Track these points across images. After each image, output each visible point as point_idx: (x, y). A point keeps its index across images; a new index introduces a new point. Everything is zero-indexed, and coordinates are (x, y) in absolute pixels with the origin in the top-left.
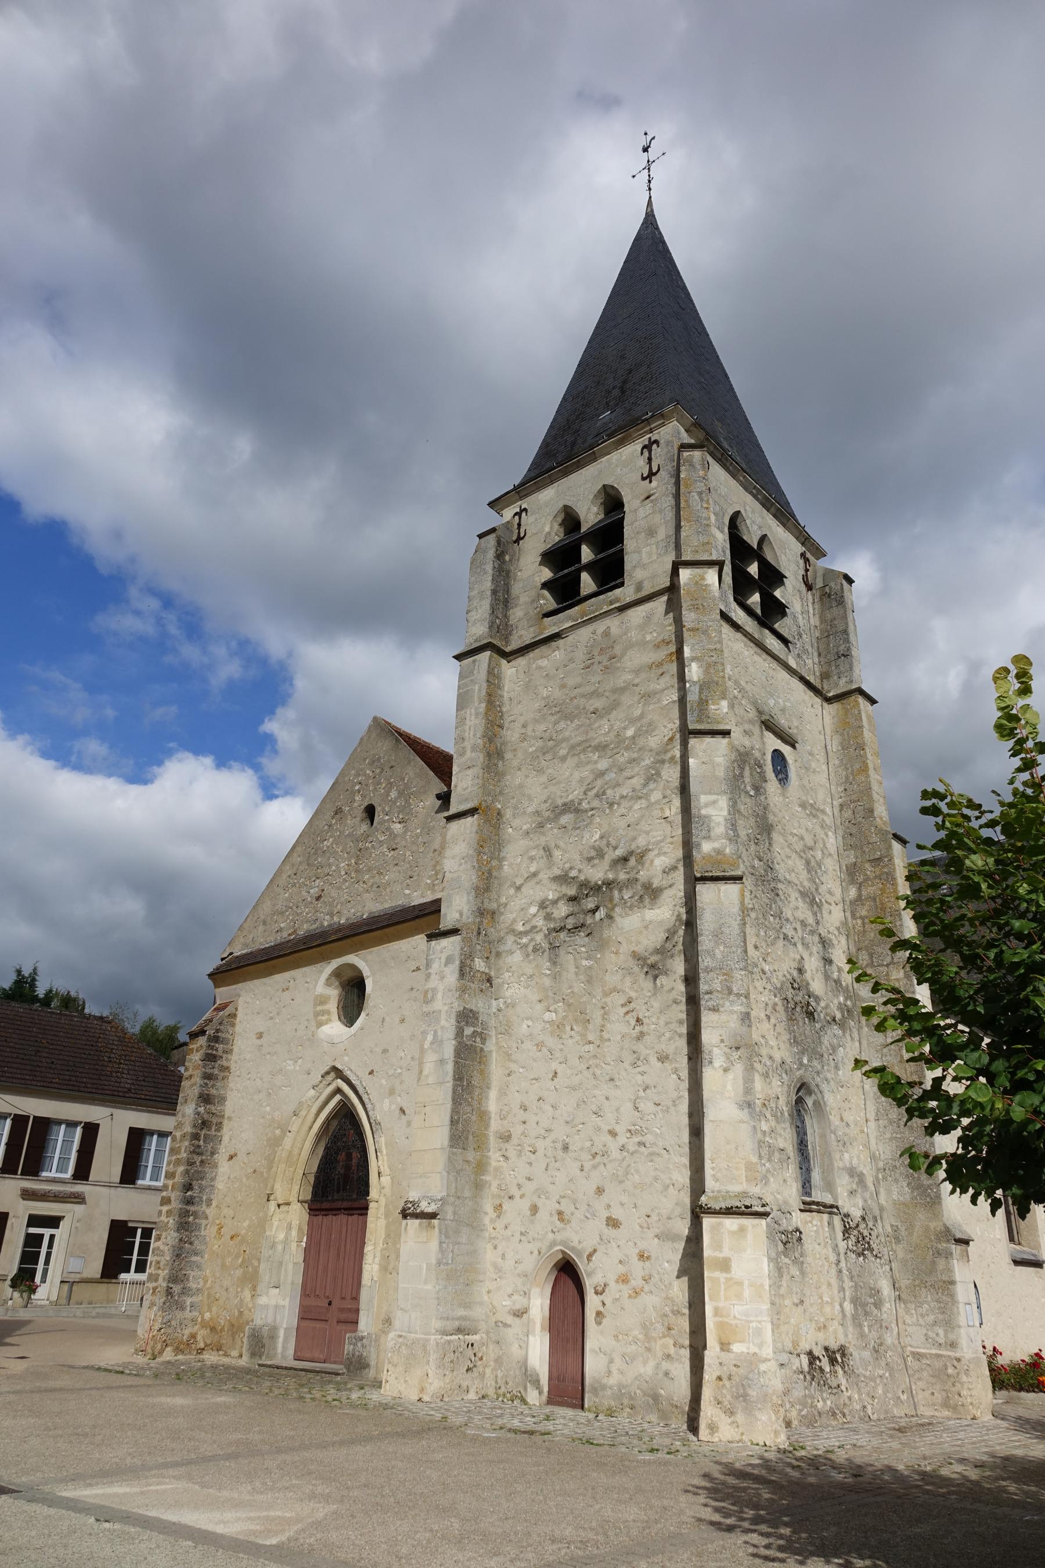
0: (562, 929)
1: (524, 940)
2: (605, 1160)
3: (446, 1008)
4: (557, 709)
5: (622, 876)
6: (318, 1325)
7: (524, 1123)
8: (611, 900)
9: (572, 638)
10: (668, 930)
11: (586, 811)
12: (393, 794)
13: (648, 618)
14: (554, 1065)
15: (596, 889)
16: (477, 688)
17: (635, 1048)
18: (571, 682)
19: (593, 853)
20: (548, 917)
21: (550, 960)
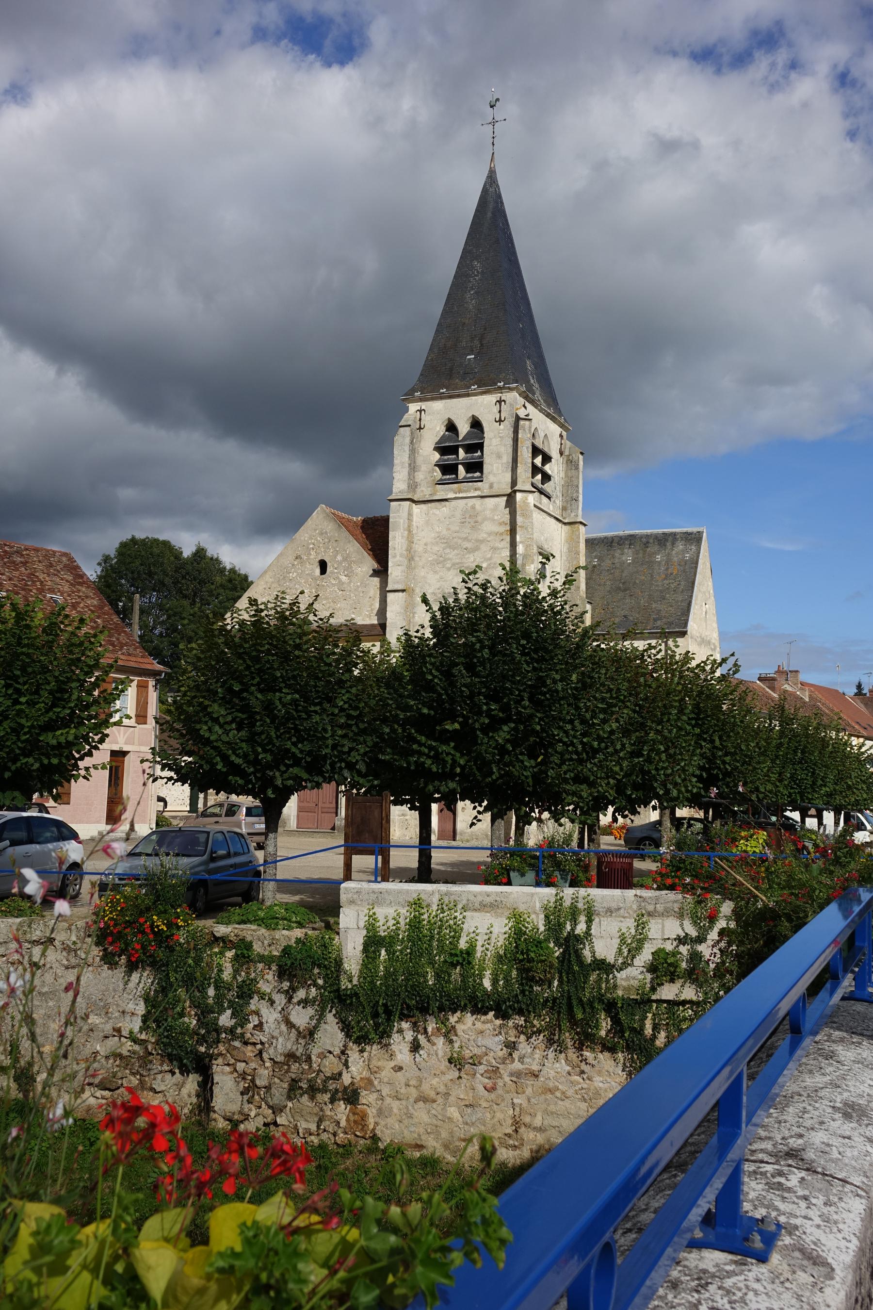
6: (310, 814)
9: (454, 503)
12: (339, 558)
13: (496, 506)
16: (402, 521)
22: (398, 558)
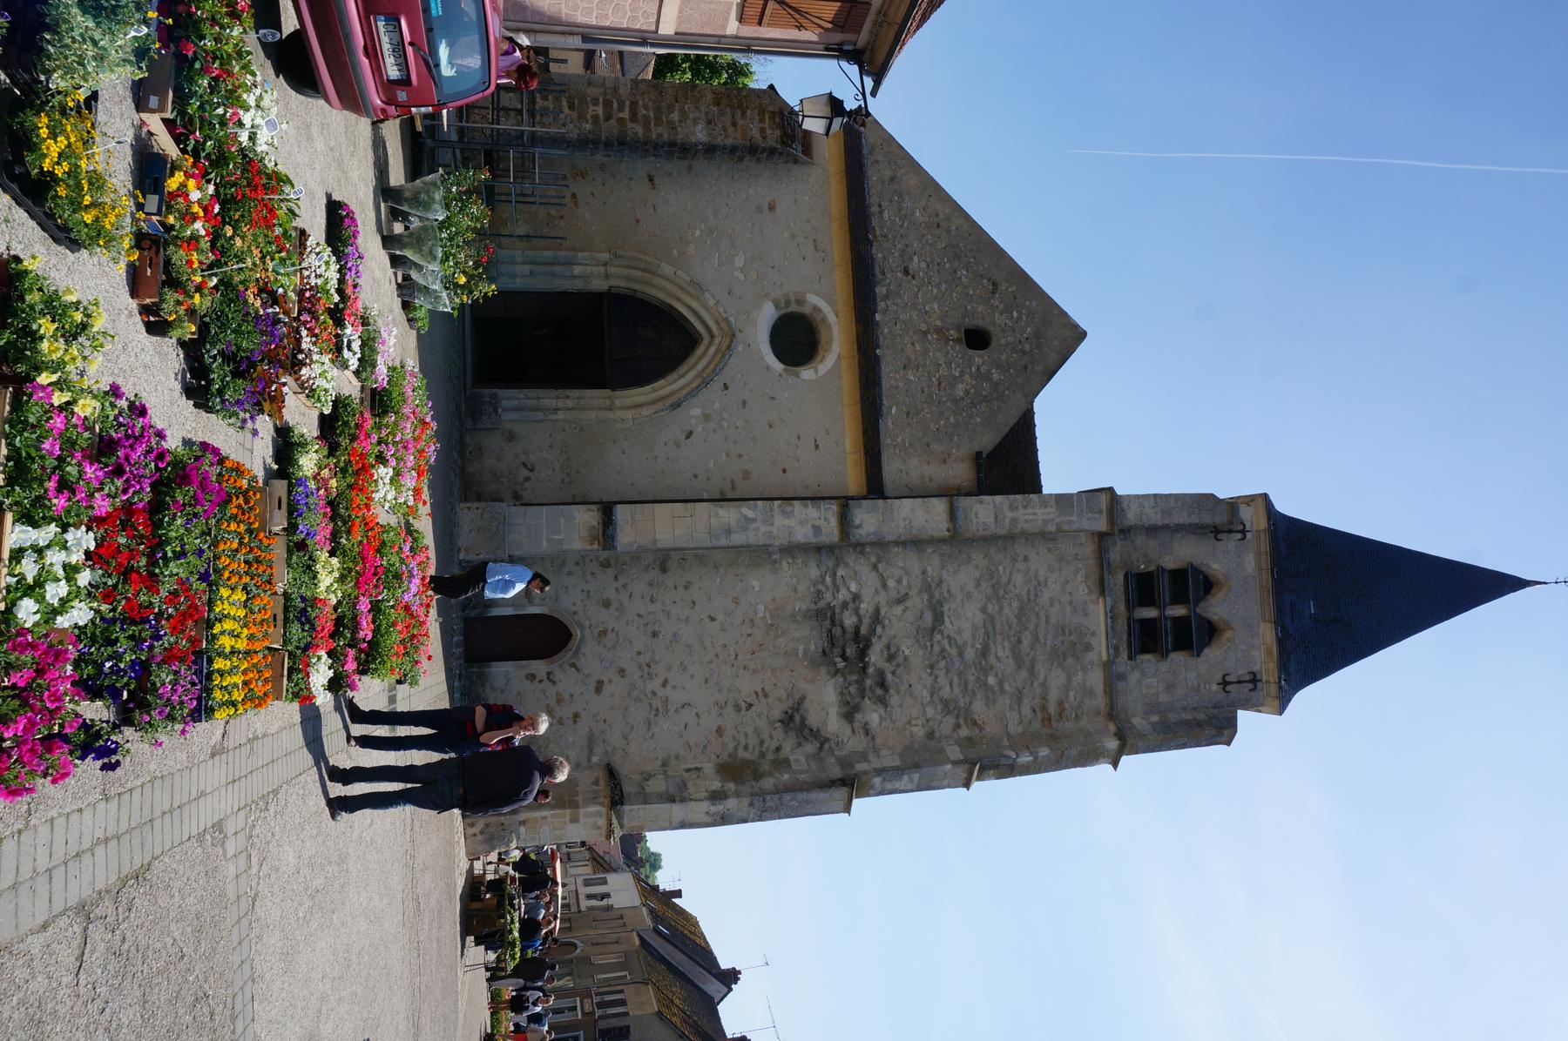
0: (833, 621)
1: (828, 579)
2: (646, 676)
3: (775, 531)
4: (1032, 598)
5: (868, 682)
7: (676, 588)
8: (851, 673)
10: (818, 731)
11: (931, 640)
14: (720, 617)
15: (863, 653)
16: (1074, 518)
17: (729, 703)
18: (1053, 611)
19: (893, 650)
20: (845, 605)
21: (808, 611)
22: (1010, 515)
